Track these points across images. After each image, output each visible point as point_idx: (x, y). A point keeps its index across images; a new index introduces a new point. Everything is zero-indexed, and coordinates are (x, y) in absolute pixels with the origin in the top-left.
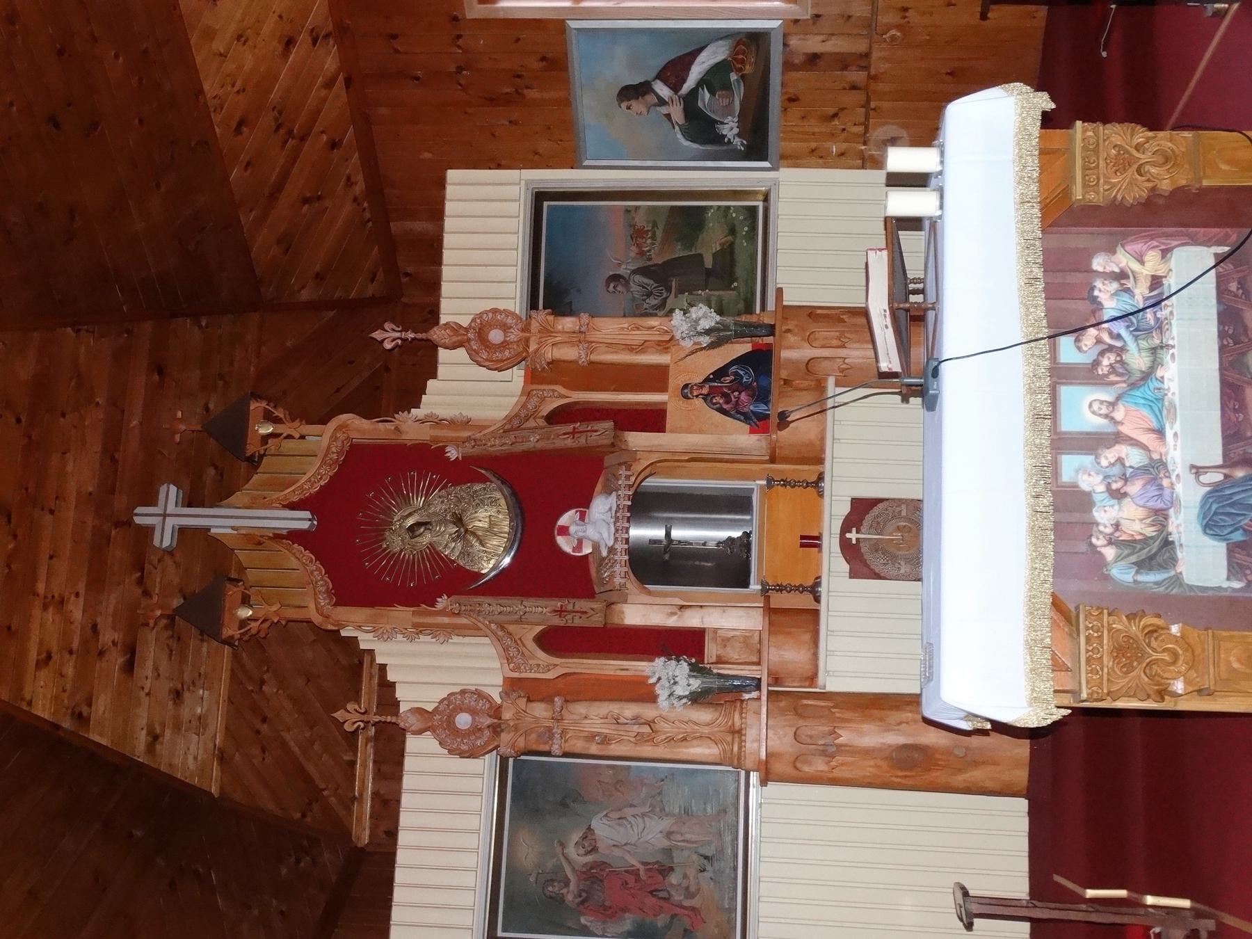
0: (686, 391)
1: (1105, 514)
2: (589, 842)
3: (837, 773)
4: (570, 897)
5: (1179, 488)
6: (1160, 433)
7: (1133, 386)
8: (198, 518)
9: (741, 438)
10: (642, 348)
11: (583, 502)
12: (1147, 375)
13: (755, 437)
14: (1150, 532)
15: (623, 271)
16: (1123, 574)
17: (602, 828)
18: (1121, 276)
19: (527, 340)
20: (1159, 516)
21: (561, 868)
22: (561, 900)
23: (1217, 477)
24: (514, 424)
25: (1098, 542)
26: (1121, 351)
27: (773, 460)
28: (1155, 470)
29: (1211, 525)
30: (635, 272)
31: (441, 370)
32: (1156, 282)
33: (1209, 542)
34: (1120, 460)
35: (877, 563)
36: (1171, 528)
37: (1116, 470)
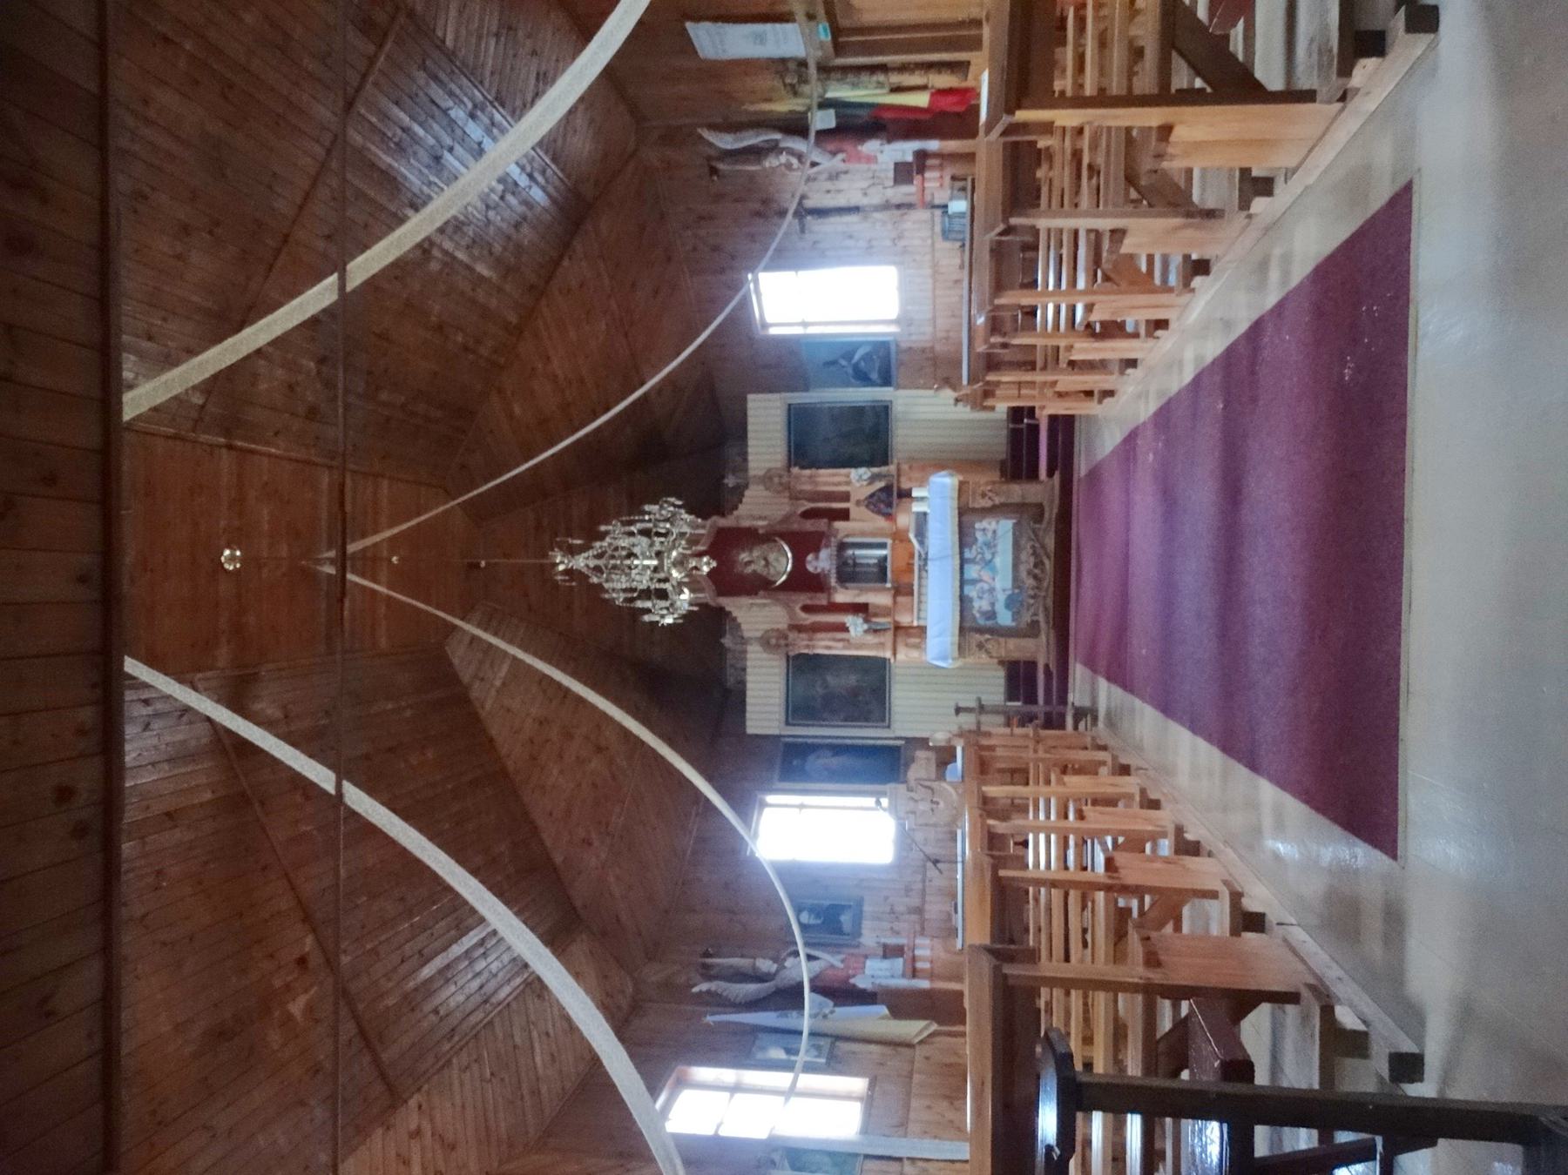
0: (858, 503)
1: (976, 604)
2: (825, 685)
6: (994, 579)
9: (881, 522)
12: (990, 561)
16: (982, 622)
17: (829, 678)
18: (984, 530)
20: (993, 604)
23: (1010, 592)
25: (975, 612)
26: (983, 554)
28: (992, 590)
29: (1008, 606)
32: (994, 532)
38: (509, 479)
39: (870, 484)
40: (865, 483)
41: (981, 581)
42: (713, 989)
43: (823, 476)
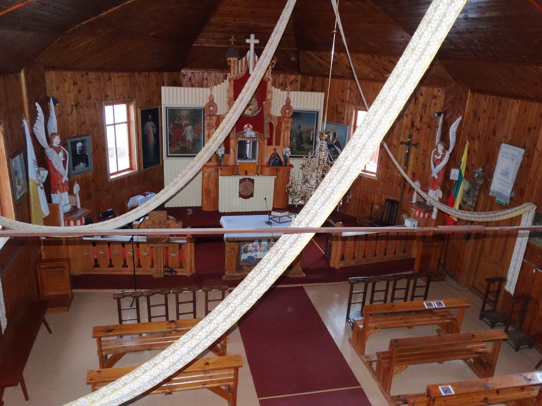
0: (275, 149)
1: (251, 245)
3: (204, 179)
4: (175, 122)
5: (254, 253)
6: (261, 251)
7: (267, 248)
8: (252, 47)
10: (284, 140)
11: (254, 129)
13: (266, 163)
14: (248, 250)
15: (301, 128)
16: (243, 247)
17: (189, 128)
19: (286, 118)
20: (250, 251)
21: (181, 120)
22: (175, 120)
23: (255, 258)
24: (270, 116)
25: (247, 244)
27: (261, 166)
28: (256, 251)
29: (249, 257)
30: (301, 131)
31: (282, 92)
33: (247, 257)
34: (257, 247)
35: (242, 184)
36: (249, 253)
37: (256, 246)
38: (344, 32)
39: (283, 155)
40: (284, 154)
41: (260, 246)
42: (39, 114)
43: (288, 132)
